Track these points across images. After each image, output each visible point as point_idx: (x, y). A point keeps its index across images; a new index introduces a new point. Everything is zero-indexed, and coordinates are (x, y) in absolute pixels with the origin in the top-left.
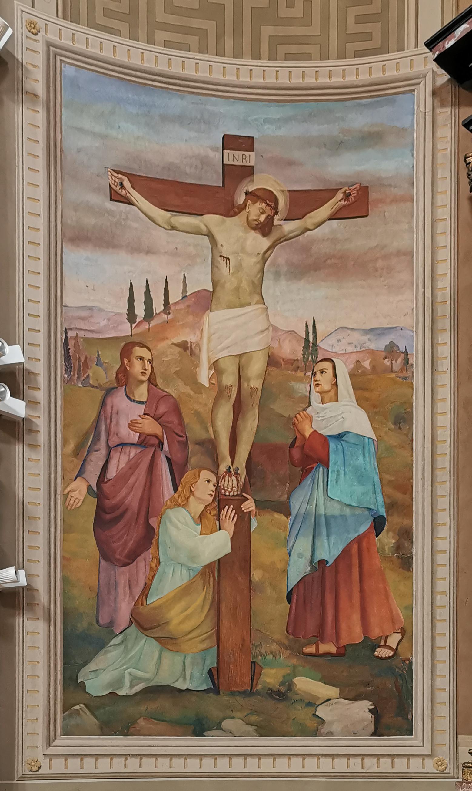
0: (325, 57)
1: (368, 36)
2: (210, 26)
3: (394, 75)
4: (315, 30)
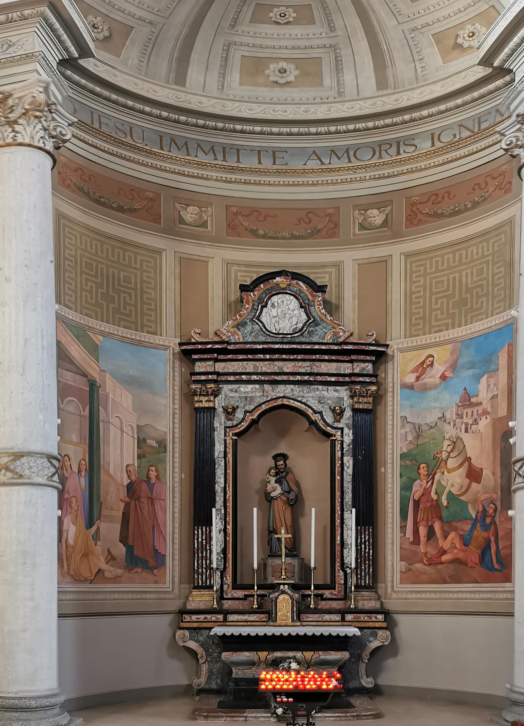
1: (500, 307)
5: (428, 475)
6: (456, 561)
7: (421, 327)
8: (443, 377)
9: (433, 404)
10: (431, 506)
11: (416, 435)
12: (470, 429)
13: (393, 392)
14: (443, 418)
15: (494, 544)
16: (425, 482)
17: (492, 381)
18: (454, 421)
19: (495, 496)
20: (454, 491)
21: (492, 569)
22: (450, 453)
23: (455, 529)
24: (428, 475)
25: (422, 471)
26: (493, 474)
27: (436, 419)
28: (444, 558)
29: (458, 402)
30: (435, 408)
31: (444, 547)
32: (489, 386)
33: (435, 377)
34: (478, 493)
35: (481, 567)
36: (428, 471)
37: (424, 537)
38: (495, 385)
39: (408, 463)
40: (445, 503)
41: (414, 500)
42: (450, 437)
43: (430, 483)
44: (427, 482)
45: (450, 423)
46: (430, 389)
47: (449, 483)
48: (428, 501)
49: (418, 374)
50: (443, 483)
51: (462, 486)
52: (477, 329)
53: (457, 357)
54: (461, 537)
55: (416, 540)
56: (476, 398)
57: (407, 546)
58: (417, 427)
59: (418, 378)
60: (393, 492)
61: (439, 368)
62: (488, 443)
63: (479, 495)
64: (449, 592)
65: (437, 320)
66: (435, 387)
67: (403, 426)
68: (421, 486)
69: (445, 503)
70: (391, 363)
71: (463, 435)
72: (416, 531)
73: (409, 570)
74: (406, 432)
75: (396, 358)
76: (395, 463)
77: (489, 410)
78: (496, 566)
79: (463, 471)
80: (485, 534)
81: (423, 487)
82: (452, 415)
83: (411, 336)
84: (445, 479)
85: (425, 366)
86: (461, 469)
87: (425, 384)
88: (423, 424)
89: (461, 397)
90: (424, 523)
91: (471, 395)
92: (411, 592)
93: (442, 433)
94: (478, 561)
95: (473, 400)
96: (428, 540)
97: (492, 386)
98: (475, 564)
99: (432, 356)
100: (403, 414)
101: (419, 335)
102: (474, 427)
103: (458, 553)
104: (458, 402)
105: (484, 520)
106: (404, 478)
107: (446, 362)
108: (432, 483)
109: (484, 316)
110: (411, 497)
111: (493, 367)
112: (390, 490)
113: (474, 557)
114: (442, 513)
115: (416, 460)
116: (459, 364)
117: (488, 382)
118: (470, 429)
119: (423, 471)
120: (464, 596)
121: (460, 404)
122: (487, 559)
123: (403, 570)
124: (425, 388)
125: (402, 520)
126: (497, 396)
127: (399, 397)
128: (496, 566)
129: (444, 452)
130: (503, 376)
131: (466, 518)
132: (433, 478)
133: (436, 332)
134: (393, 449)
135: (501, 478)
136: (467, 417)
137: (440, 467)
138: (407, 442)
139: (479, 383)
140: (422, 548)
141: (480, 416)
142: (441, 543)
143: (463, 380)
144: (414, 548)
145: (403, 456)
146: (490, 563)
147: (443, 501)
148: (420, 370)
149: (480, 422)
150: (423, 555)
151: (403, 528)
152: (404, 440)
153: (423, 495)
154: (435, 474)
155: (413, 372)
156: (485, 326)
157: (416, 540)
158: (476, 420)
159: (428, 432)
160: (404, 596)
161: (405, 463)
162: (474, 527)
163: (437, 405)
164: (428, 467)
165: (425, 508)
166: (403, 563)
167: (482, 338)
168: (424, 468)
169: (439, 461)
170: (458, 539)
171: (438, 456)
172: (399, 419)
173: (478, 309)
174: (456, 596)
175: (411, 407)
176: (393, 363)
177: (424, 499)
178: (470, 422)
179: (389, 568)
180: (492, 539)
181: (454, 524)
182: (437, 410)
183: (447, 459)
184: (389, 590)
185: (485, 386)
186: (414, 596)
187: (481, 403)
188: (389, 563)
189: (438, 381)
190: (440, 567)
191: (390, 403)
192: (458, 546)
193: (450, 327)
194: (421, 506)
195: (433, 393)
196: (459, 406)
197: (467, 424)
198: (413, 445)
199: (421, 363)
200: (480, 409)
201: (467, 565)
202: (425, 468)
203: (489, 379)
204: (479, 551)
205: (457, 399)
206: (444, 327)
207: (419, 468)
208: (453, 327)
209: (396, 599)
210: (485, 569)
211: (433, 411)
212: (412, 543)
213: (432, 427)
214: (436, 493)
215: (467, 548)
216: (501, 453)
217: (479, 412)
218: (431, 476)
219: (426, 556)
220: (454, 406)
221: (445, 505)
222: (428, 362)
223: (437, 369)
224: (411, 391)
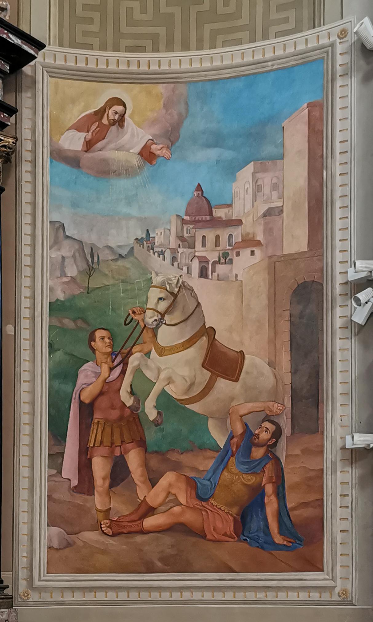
0: (253, 40)
1: (286, 20)
2: (162, 31)
3: (50, 63)
4: (244, 21)
5: (113, 355)
6: (177, 528)
7: (95, 28)
8: (147, 155)
9: (124, 209)
10: (121, 418)
11: (86, 266)
12: (213, 271)
13: (34, 162)
14: (146, 241)
15: (273, 498)
16: (105, 368)
17: (267, 179)
18: (174, 251)
19: (276, 407)
20: (175, 391)
21: (268, 544)
22: (163, 315)
23: (176, 467)
24: (112, 353)
25: (98, 344)
26: (271, 364)
27: (132, 241)
28: (149, 522)
29: (182, 214)
30: (128, 217)
31: (148, 500)
32: (258, 189)
33: (128, 151)
34: (232, 399)
35: (240, 540)
36: (112, 346)
37: (104, 479)
38: (275, 187)
39: (69, 323)
40: (151, 413)
41: (81, 403)
42: (163, 283)
43: (118, 371)
44: (111, 369)
45: (162, 253)
46: (118, 174)
47: (163, 376)
48: (113, 407)
49: (89, 136)
50: (149, 374)
51: (192, 385)
52: (226, 62)
53: (180, 114)
54: (191, 483)
55: (86, 483)
56: (226, 210)
57: (63, 495)
58: (87, 251)
59: (89, 145)
60: (32, 381)
61: (135, 135)
62: (259, 304)
63: (233, 404)
64: (160, 589)
65: (131, 22)
66: (128, 172)
67: (56, 243)
68: (98, 375)
69: (151, 413)
70: (29, 95)
71: (195, 282)
72: (85, 467)
73: (69, 545)
74: (63, 258)
75: (39, 86)
76: (38, 320)
77: (260, 237)
78: (278, 539)
79: (196, 353)
80: (251, 480)
81: (101, 379)
82: (167, 237)
83: (73, 44)
84: (153, 366)
85: (105, 121)
86: (191, 352)
87: (105, 161)
88: (100, 245)
89: (189, 204)
90: (104, 450)
91: (213, 203)
92: (72, 589)
93: (145, 271)
94: (230, 528)
95: (220, 213)
96: (111, 486)
97: (267, 190)
98: (225, 535)
99: (119, 101)
100: (56, 217)
101: (91, 47)
102: (221, 269)
103: (182, 513)
104: (182, 214)
105: (248, 452)
106: (59, 355)
107: (154, 122)
108: (123, 372)
109: (244, 35)
110: (75, 396)
111: (268, 149)
112: (25, 376)
113: (222, 521)
114: (146, 433)
115: (85, 321)
116: (184, 132)
117: (255, 180)
118: (213, 271)
119: (101, 344)
120: (197, 596)
121: (187, 218)
122: (255, 525)
123: (56, 545)
124: (105, 171)
125: (52, 442)
126: (281, 211)
127: (47, 178)
128: (278, 539)
129: (149, 313)
130: (295, 173)
131: (204, 447)
132: (125, 363)
133: (130, 49)
134: (33, 288)
135: (294, 372)
136: (204, 245)
137: (140, 340)
138: (65, 279)
139: (234, 179)
140: (99, 501)
141: (238, 248)
142: (142, 492)
143: (194, 167)
144: (79, 499)
145: (55, 308)
146: (261, 535)
147: (147, 411)
148: (93, 128)
149: (236, 259)
150: (101, 516)
151: (56, 458)
152: (58, 273)
153: (101, 393)
154: (130, 353)
155: (78, 127)
156: (248, 59)
157: (86, 483)
158: (225, 255)
159: (114, 266)
160: (57, 597)
161: (61, 322)
162: (222, 462)
163: (134, 211)
164: (112, 338)
165: (106, 421)
166: (55, 530)
167: (239, 84)
168: (103, 338)
169: (139, 330)
170: (183, 485)
171: (136, 317)
172: (47, 225)
173: (228, 17)
174: (176, 596)
175: (75, 205)
176: (34, 97)
177: (103, 402)
178: (213, 257)
179: (24, 539)
180: (269, 489)
181: (174, 457)
182: (132, 223)
183: (158, 327)
184: (22, 585)
185: (250, 187)
186: (78, 596)
187: (239, 222)
188: (24, 529)
189: (135, 161)
190: (139, 539)
191: (26, 188)
192: (182, 499)
193: (162, 46)
194: (98, 416)
195: (122, 184)
196: (184, 222)
197: (203, 261)
198: (80, 287)
199: (96, 113)
200: (237, 234)
201: (204, 537)
202: (107, 340)
203: (259, 175)
204: (235, 510)
205: (179, 205)
206: (149, 43)
207: (92, 338)
208: (170, 48)
209: (36, 604)
210: (250, 544)
211: (124, 223)
212: (77, 490)
213: (121, 256)
214: (132, 393)
215: (204, 504)
216: (292, 324)
217: (234, 240)
218: (120, 356)
219: (107, 517)
220: (174, 220)
221: (152, 418)
222: (112, 114)
223: (133, 135)
224: (75, 171)
